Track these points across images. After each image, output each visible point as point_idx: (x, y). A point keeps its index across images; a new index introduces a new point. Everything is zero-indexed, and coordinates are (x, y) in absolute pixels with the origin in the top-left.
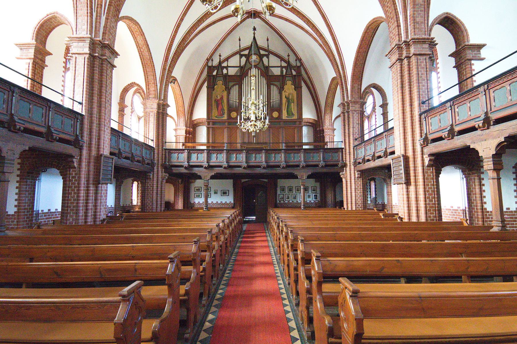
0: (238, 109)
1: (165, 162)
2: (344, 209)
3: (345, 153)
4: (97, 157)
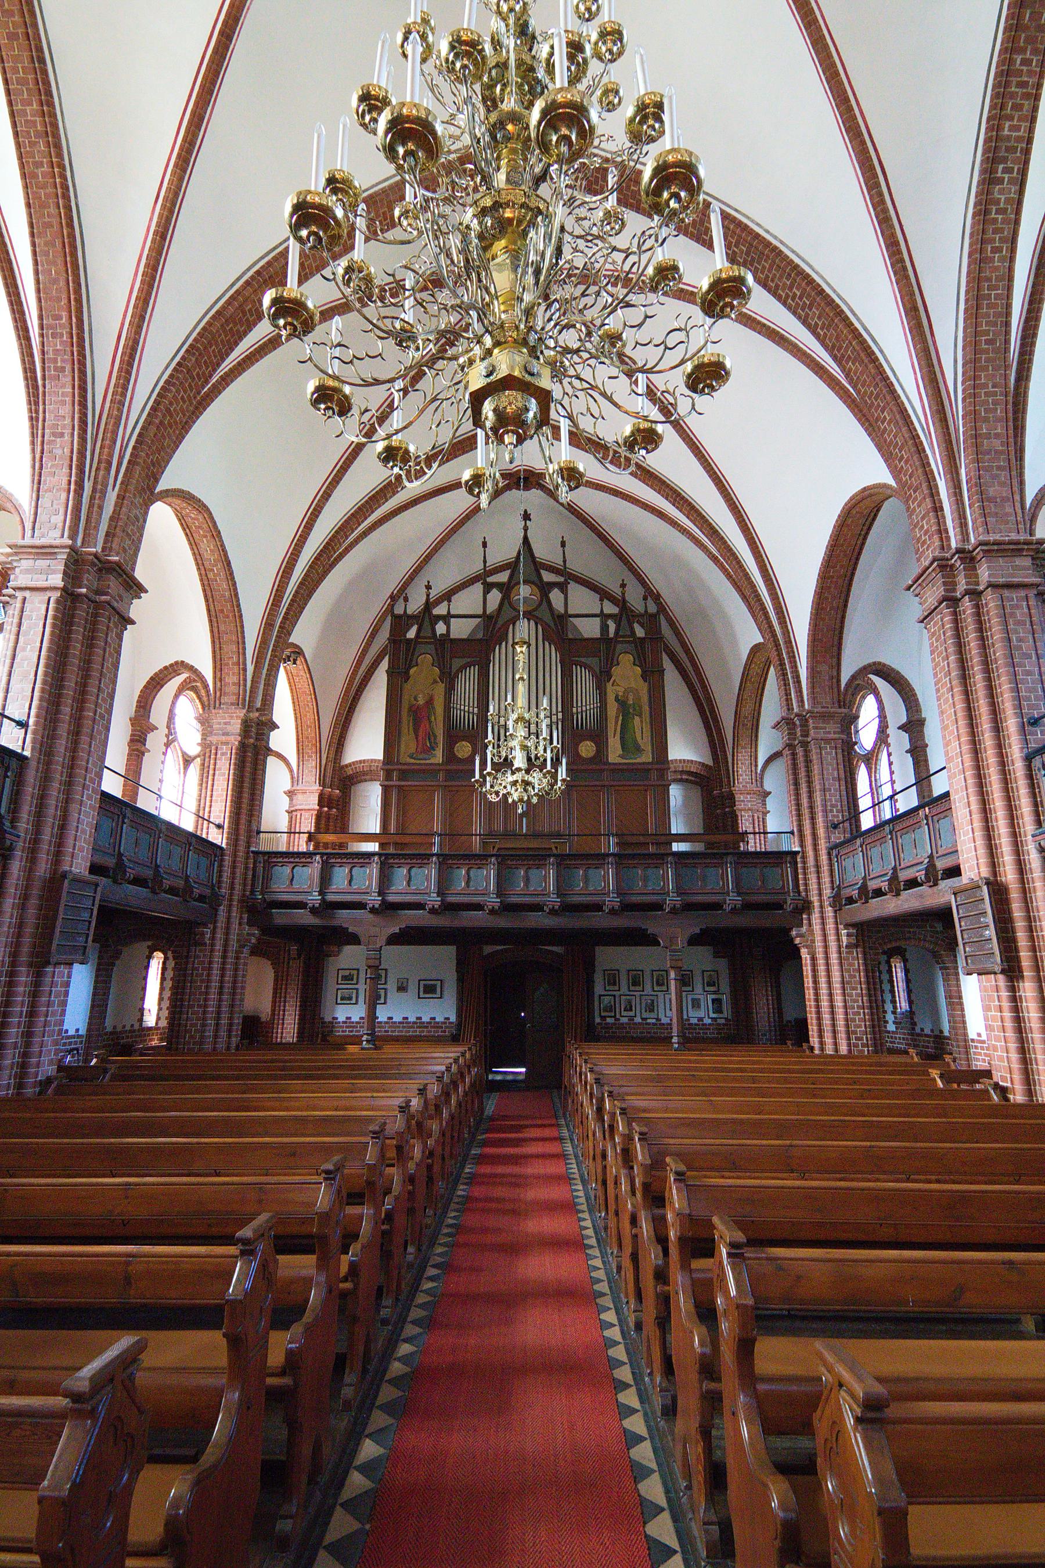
0: (476, 735)
1: (252, 892)
2: (812, 1049)
3: (804, 868)
4: (52, 879)
